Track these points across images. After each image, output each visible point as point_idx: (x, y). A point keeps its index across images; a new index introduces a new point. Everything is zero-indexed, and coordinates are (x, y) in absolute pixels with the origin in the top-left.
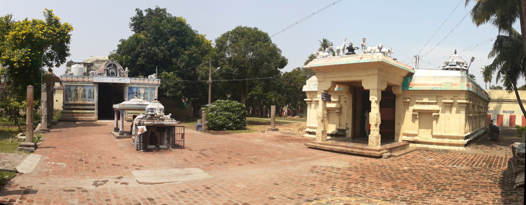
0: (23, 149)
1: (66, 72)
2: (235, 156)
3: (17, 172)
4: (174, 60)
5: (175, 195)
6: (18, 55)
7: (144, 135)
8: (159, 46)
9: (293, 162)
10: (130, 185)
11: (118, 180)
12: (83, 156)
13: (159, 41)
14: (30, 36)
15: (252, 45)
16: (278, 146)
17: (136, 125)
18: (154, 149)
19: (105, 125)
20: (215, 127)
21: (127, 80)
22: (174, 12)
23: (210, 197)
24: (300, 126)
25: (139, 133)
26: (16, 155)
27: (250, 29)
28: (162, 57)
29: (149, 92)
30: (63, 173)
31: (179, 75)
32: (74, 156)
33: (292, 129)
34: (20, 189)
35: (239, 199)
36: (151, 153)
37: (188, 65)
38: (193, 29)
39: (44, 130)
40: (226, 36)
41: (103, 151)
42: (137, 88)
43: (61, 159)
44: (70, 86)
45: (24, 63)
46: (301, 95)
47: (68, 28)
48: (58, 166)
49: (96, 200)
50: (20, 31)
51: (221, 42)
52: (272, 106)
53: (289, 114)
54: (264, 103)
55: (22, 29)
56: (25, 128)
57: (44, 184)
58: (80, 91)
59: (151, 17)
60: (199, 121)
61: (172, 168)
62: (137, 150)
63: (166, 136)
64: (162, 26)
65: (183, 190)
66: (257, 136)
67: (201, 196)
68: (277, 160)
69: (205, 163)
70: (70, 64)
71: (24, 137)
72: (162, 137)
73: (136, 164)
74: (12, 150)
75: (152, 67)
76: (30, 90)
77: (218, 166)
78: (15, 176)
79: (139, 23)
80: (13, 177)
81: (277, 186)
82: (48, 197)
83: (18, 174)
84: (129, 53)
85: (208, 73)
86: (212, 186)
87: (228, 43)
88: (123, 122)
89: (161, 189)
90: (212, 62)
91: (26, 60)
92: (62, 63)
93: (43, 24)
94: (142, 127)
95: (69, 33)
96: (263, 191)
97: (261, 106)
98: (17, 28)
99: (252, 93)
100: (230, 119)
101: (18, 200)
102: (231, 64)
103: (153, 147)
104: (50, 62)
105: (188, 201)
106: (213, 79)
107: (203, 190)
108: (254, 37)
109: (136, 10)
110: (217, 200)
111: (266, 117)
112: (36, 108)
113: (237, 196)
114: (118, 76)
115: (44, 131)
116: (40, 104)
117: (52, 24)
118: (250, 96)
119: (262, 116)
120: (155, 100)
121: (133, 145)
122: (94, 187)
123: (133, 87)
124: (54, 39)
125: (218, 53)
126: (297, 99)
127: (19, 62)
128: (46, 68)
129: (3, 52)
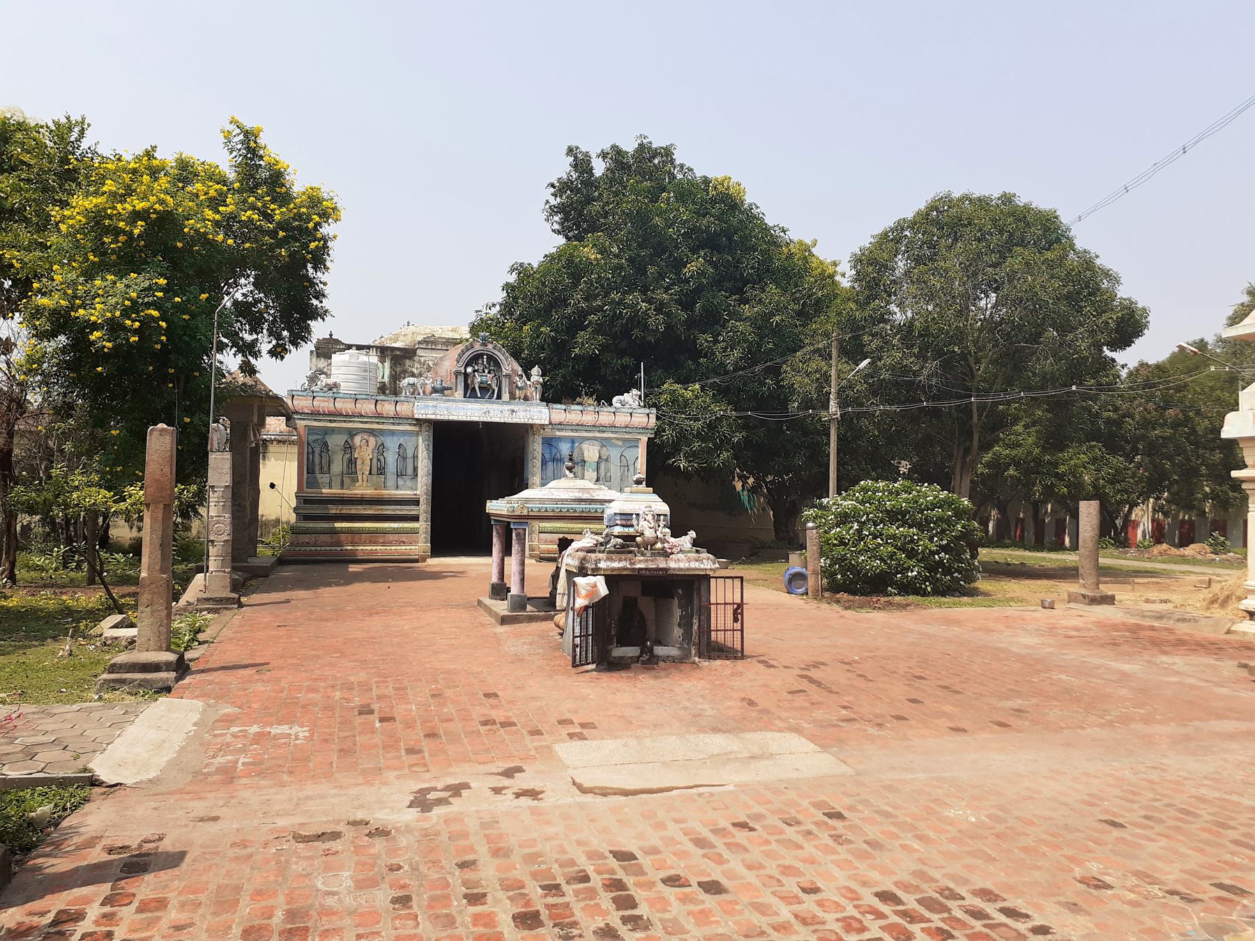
0: (123, 681)
1: (313, 379)
2: (937, 696)
3: (94, 782)
4: (704, 339)
5: (713, 838)
6: (107, 299)
7: (599, 609)
8: (648, 283)
9: (1187, 738)
10: (549, 800)
11: (506, 782)
12: (375, 692)
13: (651, 270)
14: (163, 225)
15: (994, 266)
16: (1115, 665)
17: (570, 574)
18: (636, 660)
19: (456, 574)
20: (854, 583)
21: (536, 413)
22: (701, 158)
23: (843, 853)
24: (1216, 588)
25: (580, 602)
26: (90, 711)
27: (982, 203)
28: (662, 328)
29: (614, 454)
30: (296, 765)
31: (723, 393)
32: (338, 694)
33: (1174, 597)
34: (105, 857)
35: (956, 868)
36: (623, 674)
37: (753, 356)
38: (770, 221)
39: (219, 601)
40: (890, 240)
41: (449, 672)
42: (573, 441)
43: (287, 711)
44: (327, 431)
45: (135, 332)
46: (1218, 456)
47: (320, 208)
48: (276, 737)
49: (423, 869)
50: (122, 198)
51: (872, 264)
52: (1083, 505)
53: (1159, 535)
54: (1049, 492)
55: (129, 192)
56: (135, 594)
57: (215, 819)
58: (365, 451)
59: (621, 183)
60: (794, 557)
61: (702, 730)
62: (574, 665)
63: (677, 613)
64: (660, 213)
65: (743, 818)
66: (1022, 619)
67: (809, 848)
68: (1110, 724)
69: (819, 714)
70: (327, 349)
71: (132, 632)
72: (662, 616)
73: (568, 716)
74: (75, 689)
75: (625, 367)
76: (160, 442)
77: (872, 731)
78: (86, 800)
79: (578, 203)
80: (75, 807)
81: (1116, 833)
82: (229, 874)
83: (97, 790)
84: (543, 314)
85: (827, 381)
86: (851, 808)
87: (901, 264)
88: (523, 564)
89: (661, 815)
90: (841, 342)
91: (147, 322)
92: (296, 345)
93: (223, 181)
94: (591, 579)
95: (325, 230)
96: (1057, 847)
97: (1036, 507)
98: (109, 186)
99: (997, 456)
100: (911, 554)
101: (94, 911)
102: (910, 347)
103: (631, 651)
104: (248, 338)
105: (761, 867)
106: (843, 404)
107: (817, 824)
108: (1001, 232)
109: (570, 151)
110: (873, 867)
111: (1058, 547)
112: (185, 515)
113: (949, 855)
114: (506, 396)
115: (217, 604)
116: (201, 497)
117: (257, 186)
118: (988, 465)
119: (1039, 545)
120: (638, 482)
121: (559, 647)
122: (414, 813)
123: (560, 439)
124: (262, 248)
125: (862, 305)
126: (1195, 472)
127: (114, 327)
128: (230, 361)
129: (38, 277)
